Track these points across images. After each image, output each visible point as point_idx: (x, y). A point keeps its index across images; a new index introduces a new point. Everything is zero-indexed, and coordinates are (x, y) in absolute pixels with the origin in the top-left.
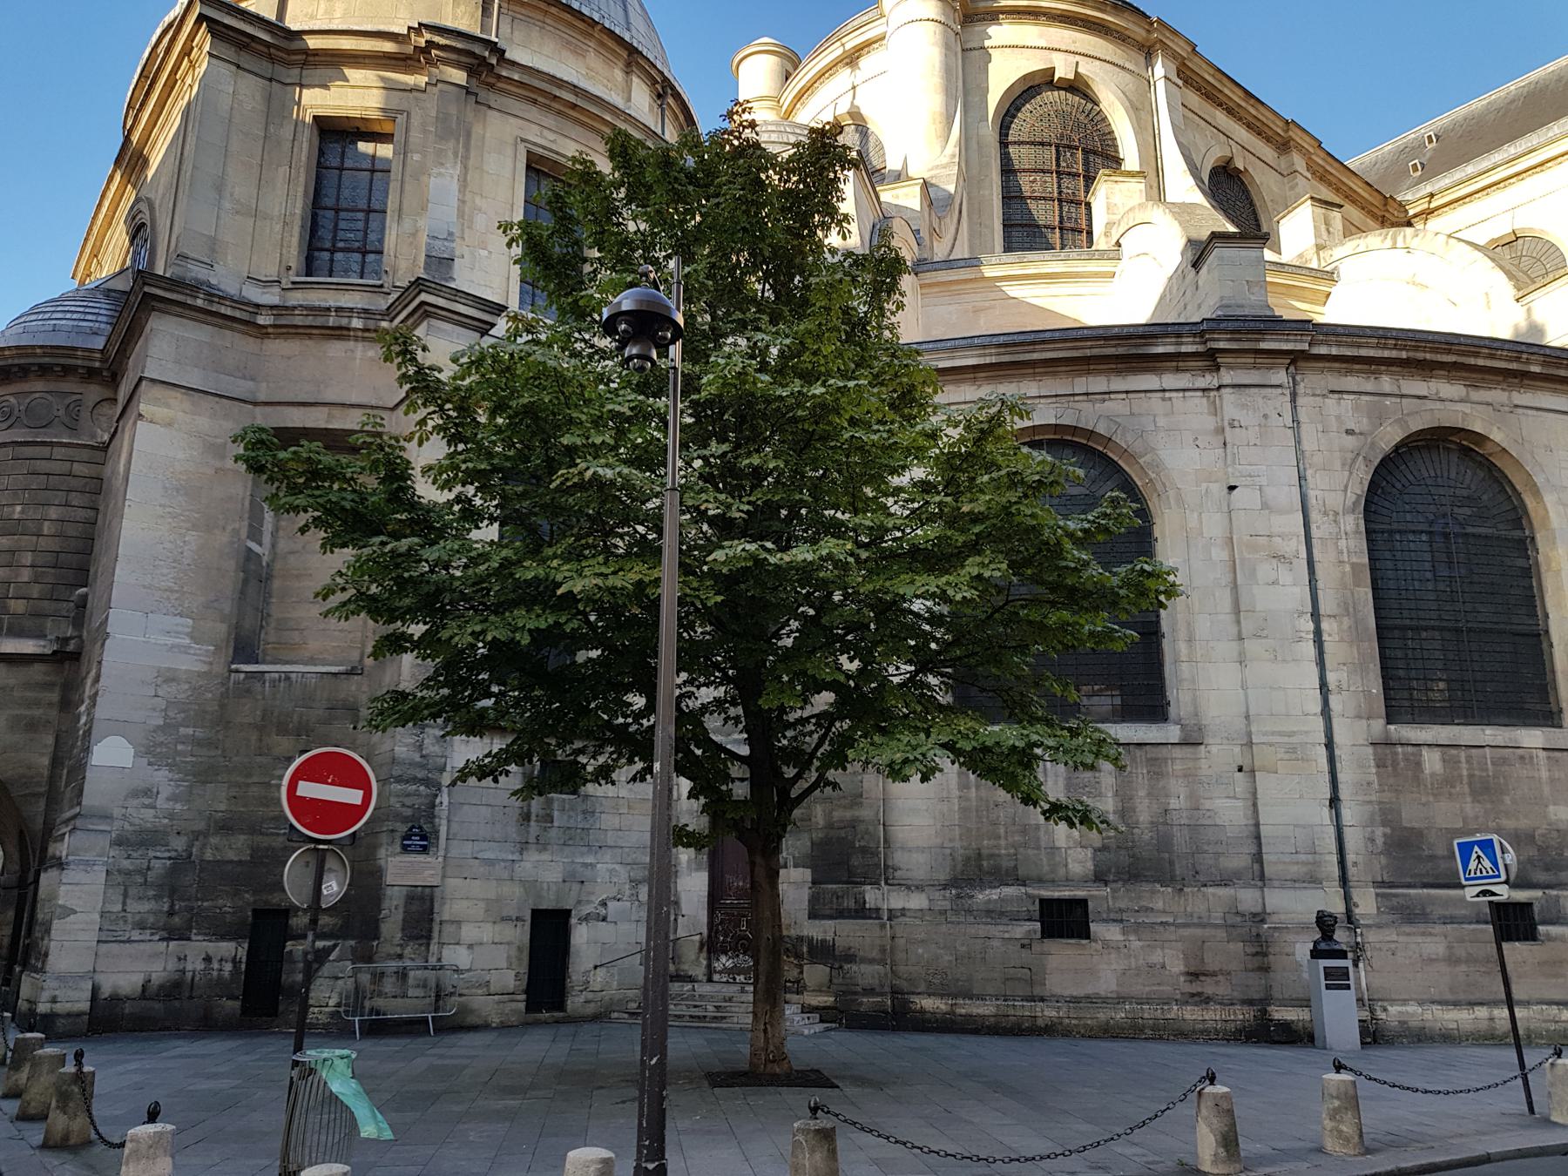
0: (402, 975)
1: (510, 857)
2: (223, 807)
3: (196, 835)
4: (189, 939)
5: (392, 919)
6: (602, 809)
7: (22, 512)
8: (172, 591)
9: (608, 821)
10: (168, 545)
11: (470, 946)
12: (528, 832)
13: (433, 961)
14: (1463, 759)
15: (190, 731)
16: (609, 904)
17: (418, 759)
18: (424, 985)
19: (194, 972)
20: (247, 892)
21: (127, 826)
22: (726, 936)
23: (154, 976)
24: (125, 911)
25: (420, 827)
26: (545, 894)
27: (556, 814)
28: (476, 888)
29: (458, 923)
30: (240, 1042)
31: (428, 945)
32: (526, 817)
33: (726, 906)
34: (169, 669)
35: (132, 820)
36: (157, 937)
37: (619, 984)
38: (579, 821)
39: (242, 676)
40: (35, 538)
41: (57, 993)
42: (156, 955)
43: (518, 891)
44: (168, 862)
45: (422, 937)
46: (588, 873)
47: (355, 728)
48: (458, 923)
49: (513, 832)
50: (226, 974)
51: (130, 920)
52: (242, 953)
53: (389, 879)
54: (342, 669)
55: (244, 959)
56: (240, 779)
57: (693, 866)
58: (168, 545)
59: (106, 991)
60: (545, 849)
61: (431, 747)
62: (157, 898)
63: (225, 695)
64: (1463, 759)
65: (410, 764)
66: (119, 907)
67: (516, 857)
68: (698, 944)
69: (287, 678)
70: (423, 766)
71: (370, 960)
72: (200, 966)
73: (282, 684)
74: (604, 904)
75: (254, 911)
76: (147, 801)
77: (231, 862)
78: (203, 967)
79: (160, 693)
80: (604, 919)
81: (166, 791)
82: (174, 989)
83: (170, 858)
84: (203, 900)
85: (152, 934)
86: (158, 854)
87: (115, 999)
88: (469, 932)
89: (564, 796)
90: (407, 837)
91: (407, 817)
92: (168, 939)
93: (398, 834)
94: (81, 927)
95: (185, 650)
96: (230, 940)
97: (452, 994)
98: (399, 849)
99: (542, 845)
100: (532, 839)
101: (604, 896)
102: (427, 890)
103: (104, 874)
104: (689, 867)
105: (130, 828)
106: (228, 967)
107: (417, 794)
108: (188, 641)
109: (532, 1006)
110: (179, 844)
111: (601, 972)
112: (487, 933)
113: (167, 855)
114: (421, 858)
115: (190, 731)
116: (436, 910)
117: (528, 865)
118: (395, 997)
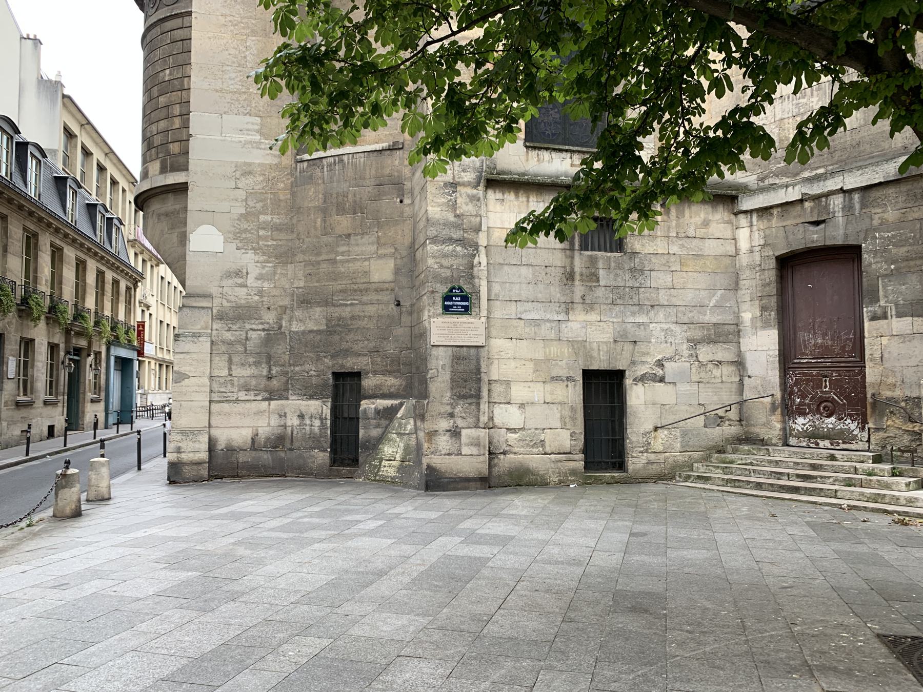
0: (455, 433)
1: (556, 318)
2: (302, 284)
3: (284, 309)
4: (287, 399)
5: (440, 379)
6: (651, 267)
7: (170, 74)
8: (240, 93)
9: (660, 279)
10: (233, 52)
11: (522, 406)
12: (573, 292)
13: (484, 419)
14: (197, 445)
15: (269, 218)
16: (666, 364)
17: (451, 218)
18: (476, 443)
19: (292, 426)
20: (325, 357)
21: (225, 304)
22: (803, 397)
23: (260, 431)
24: (231, 375)
25: (460, 288)
26: (595, 354)
27: (602, 273)
28: (524, 348)
29: (508, 383)
30: (300, 497)
31: (478, 404)
32: (570, 276)
33: (800, 366)
34: (245, 164)
35: (229, 297)
36: (260, 398)
37: (682, 447)
38: (625, 279)
39: (305, 164)
40: (179, 93)
41: (180, 444)
42: (259, 413)
43: (566, 351)
44: (263, 334)
45: (471, 396)
46: (641, 333)
47: (401, 202)
48: (508, 383)
49: (556, 292)
50: (316, 430)
51: (236, 383)
52: (327, 411)
53: (434, 339)
54: (385, 145)
55: (329, 417)
56: (313, 258)
57: (759, 324)
58: (233, 52)
59: (221, 445)
60: (592, 309)
61: (465, 207)
62: (257, 364)
63: (293, 185)
64: (197, 445)
65: (444, 225)
66: (225, 372)
67: (561, 317)
68: (769, 406)
69: (341, 161)
70: (457, 226)
71: (422, 418)
72: (296, 422)
73: (337, 167)
74: (660, 364)
75: (334, 374)
76: (240, 281)
77: (311, 331)
78: (298, 423)
79: (240, 186)
80: (662, 380)
81: (254, 271)
82: (279, 441)
83: (264, 330)
84: (294, 365)
85: (256, 395)
86: (254, 327)
87: (231, 450)
88: (519, 392)
89: (609, 254)
90: (447, 298)
91: (447, 278)
92: (269, 399)
93: (440, 295)
94: (194, 389)
95: (257, 145)
96: (317, 399)
97: (504, 453)
98: (440, 310)
99: (589, 306)
100: (577, 298)
101: (659, 357)
102: (473, 351)
103: (209, 344)
104: (754, 327)
105: (229, 305)
106: (317, 423)
107: (455, 255)
108: (258, 137)
109: (589, 465)
110: (270, 317)
111: (662, 434)
112: (538, 392)
113: (261, 327)
114: (464, 319)
115: (269, 218)
116: (483, 370)
117: (574, 325)
118: (449, 454)
